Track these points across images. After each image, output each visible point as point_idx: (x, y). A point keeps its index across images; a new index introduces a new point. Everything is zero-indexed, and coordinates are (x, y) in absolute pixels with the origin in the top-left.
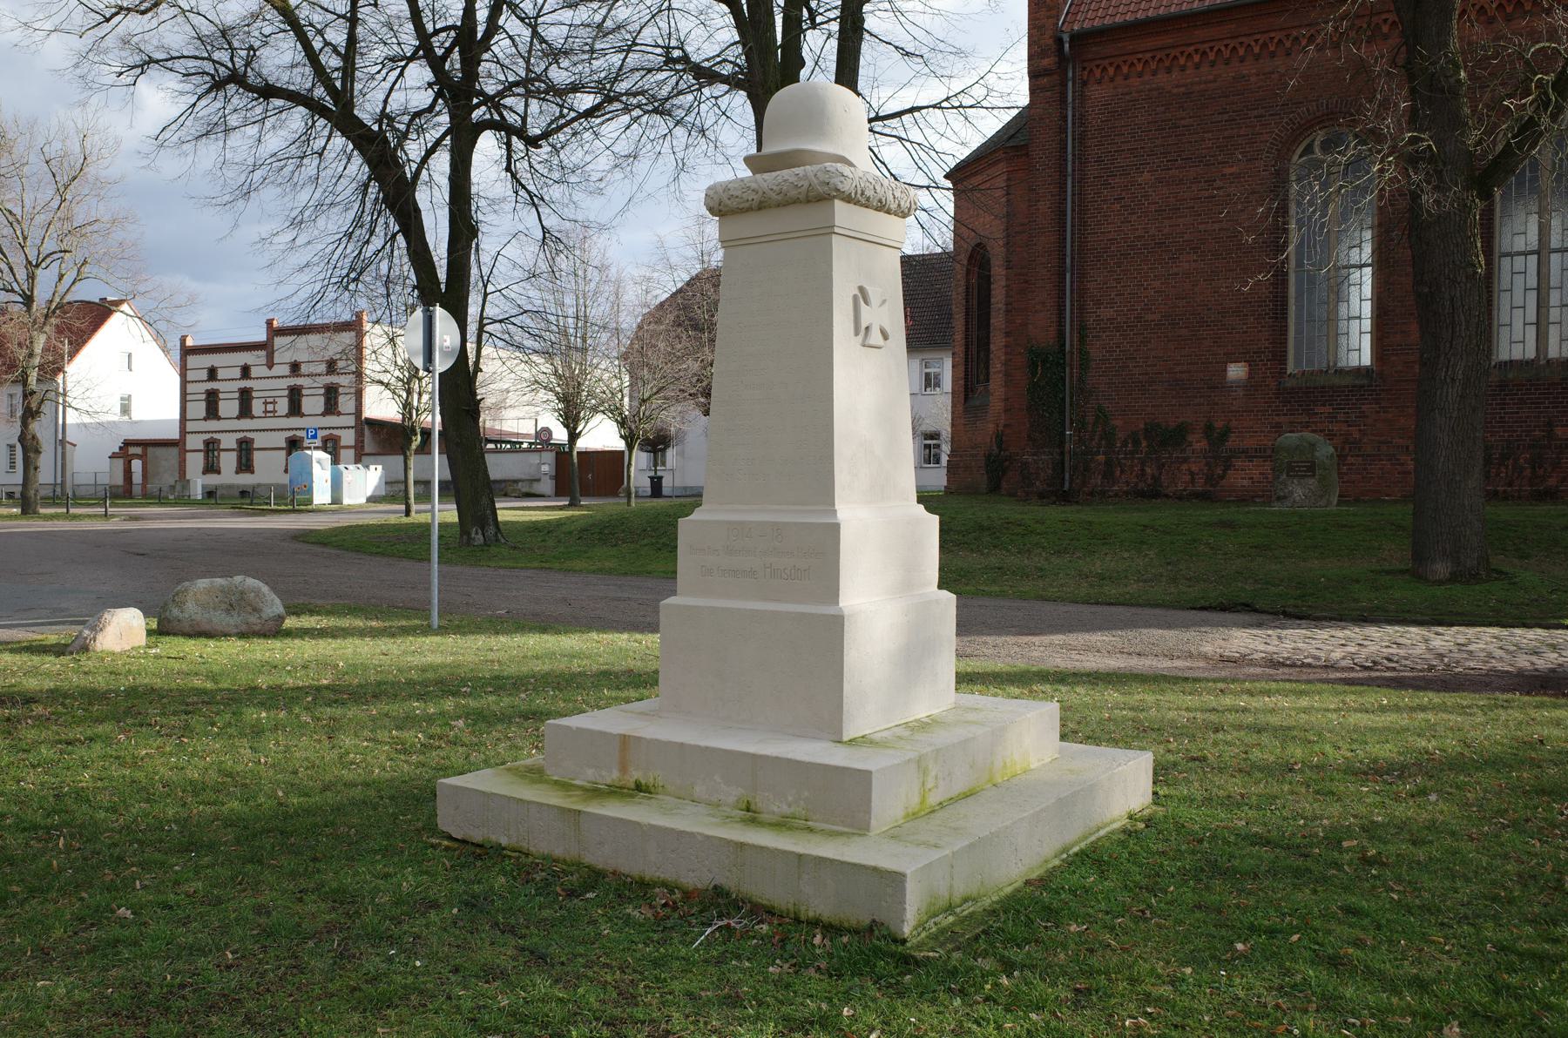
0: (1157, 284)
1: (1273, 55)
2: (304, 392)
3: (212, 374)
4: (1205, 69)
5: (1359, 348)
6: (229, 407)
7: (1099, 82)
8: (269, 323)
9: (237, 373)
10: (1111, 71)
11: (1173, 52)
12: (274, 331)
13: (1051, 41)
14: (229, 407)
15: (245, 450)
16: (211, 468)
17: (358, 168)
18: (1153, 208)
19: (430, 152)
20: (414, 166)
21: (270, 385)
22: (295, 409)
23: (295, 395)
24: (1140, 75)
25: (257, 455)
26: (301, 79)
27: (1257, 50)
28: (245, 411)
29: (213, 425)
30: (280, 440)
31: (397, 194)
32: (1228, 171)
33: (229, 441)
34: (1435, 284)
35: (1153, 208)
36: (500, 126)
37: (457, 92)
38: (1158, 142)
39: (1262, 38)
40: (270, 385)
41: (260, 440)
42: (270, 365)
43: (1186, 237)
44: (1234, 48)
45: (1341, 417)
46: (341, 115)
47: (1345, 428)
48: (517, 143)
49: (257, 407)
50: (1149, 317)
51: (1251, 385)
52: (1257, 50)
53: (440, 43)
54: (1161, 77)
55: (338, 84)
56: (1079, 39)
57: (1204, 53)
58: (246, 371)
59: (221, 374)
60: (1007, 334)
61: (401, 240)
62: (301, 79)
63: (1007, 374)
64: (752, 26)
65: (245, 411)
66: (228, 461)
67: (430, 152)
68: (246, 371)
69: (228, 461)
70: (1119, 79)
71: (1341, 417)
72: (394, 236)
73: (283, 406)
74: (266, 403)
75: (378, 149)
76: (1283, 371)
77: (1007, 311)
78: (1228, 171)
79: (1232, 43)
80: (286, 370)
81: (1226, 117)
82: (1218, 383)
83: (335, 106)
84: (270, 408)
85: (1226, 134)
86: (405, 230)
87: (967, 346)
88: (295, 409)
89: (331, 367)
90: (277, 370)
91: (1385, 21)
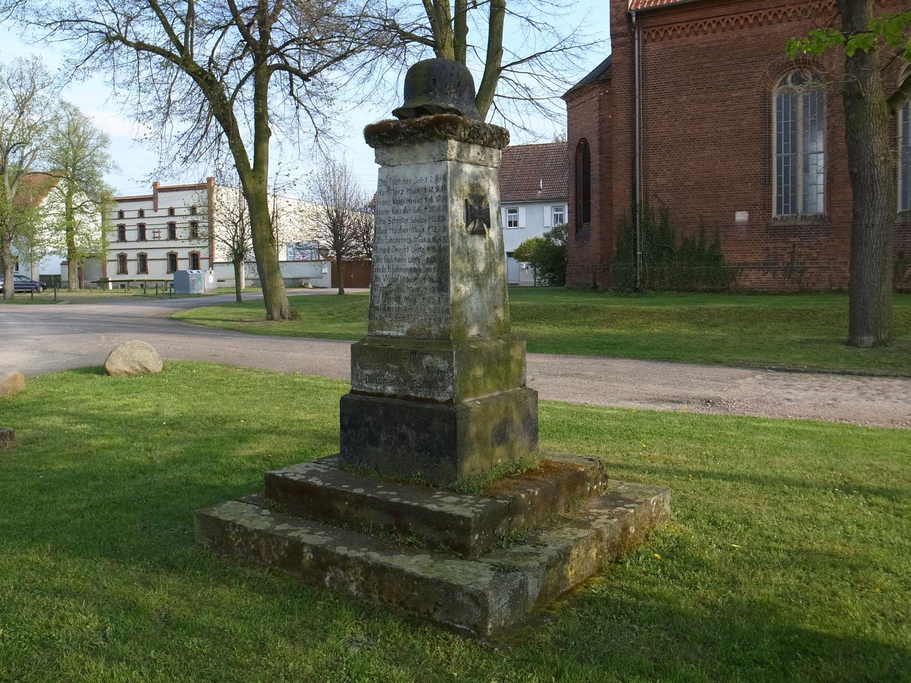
0: (692, 163)
1: (761, 24)
2: (177, 226)
3: (121, 214)
4: (719, 33)
5: (820, 205)
6: (132, 234)
7: (654, 41)
8: (155, 185)
9: (136, 214)
10: (662, 34)
11: (700, 23)
12: (158, 190)
13: (624, 16)
14: (132, 234)
15: (143, 260)
16: (123, 270)
17: (199, 96)
18: (688, 117)
19: (242, 82)
20: (232, 91)
21: (156, 222)
22: (172, 236)
23: (172, 227)
24: (705, 33)
25: (149, 264)
26: (162, 40)
27: (751, 21)
28: (142, 237)
29: (122, 245)
30: (163, 254)
31: (222, 111)
32: (734, 95)
33: (132, 255)
34: (852, 171)
35: (688, 117)
36: (285, 67)
37: (259, 49)
38: (691, 77)
39: (754, 14)
40: (156, 222)
41: (151, 255)
42: (156, 210)
43: (710, 135)
44: (737, 20)
45: (805, 244)
46: (185, 62)
47: (807, 250)
48: (298, 80)
49: (149, 235)
50: (688, 184)
51: (750, 225)
52: (751, 21)
53: (245, 18)
54: (692, 39)
55: (182, 42)
56: (643, 14)
57: (675, 30)
58: (141, 213)
59: (126, 215)
60: (601, 193)
61: (224, 137)
62: (162, 40)
63: (601, 217)
64: (435, 10)
65: (142, 237)
66: (132, 267)
67: (242, 82)
68: (141, 213)
69: (132, 267)
70: (666, 40)
71: (805, 244)
72: (220, 135)
73: (164, 234)
74: (154, 232)
75: (207, 80)
76: (770, 217)
77: (601, 180)
78: (734, 95)
79: (736, 17)
80: (166, 213)
81: (733, 62)
82: (731, 224)
83: (180, 57)
84: (157, 235)
85: (734, 72)
86: (227, 130)
87: (576, 199)
88: (172, 236)
89: (193, 210)
90: (159, 213)
91: (780, 11)
